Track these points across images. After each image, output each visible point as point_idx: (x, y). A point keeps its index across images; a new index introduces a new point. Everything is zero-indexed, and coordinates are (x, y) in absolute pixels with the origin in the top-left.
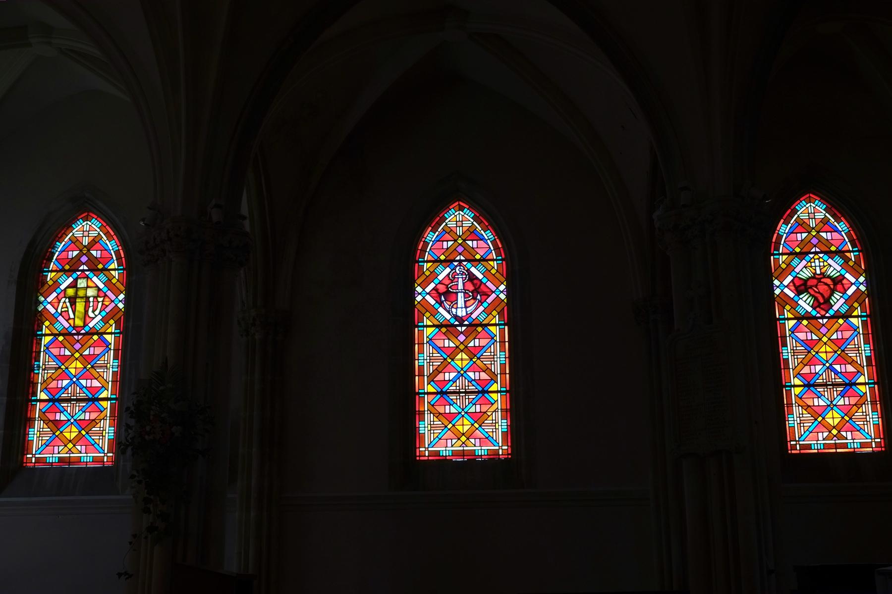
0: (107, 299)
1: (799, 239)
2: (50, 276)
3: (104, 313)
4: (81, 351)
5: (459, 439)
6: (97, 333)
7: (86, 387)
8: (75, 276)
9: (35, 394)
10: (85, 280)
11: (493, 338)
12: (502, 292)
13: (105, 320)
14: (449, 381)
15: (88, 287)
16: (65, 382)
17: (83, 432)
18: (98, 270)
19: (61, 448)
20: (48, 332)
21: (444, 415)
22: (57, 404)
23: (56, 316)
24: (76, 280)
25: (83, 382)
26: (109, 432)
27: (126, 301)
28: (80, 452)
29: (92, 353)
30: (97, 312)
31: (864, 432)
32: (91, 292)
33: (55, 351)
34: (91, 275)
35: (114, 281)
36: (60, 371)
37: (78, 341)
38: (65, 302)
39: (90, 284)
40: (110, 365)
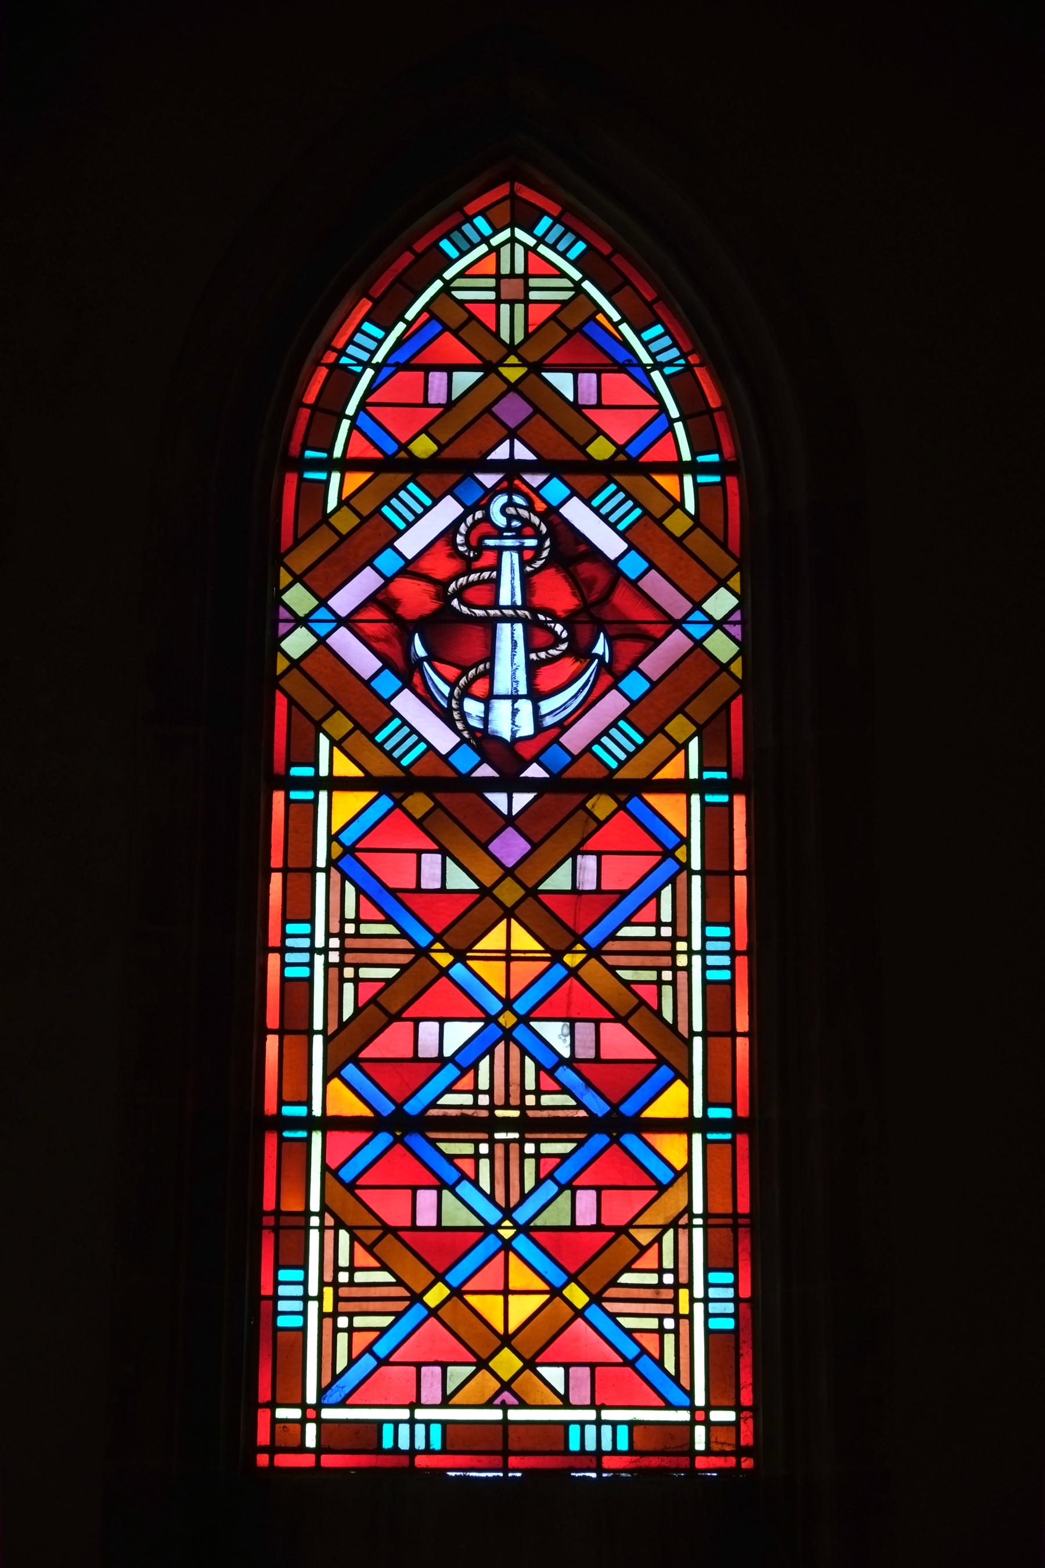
5: (482, 1364)
11: (668, 853)
12: (718, 625)
14: (441, 1061)
17: (577, 1296)
19: (457, 1374)
26: (712, 1300)
28: (566, 1403)
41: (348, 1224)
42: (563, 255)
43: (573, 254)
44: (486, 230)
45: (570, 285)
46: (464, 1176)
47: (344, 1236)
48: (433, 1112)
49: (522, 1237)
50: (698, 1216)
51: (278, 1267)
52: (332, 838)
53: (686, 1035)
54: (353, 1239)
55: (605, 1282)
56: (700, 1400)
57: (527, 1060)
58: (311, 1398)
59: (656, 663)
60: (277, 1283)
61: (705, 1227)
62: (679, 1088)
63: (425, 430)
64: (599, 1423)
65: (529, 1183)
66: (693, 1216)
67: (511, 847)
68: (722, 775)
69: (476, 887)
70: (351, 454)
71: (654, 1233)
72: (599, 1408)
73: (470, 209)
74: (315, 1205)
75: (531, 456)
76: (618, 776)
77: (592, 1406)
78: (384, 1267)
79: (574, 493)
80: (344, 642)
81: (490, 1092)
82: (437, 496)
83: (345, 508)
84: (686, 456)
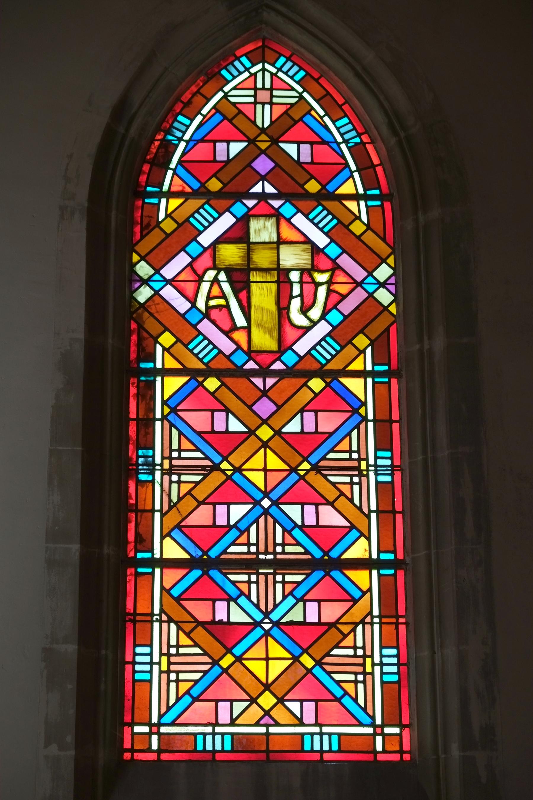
0: (341, 278)
1: (221, 156)
2: (166, 207)
3: (335, 317)
4: (276, 422)
5: (253, 700)
6: (321, 372)
7: (303, 527)
8: (239, 209)
9: (144, 542)
10: (271, 223)
11: (355, 411)
12: (382, 285)
13: (341, 335)
14: (229, 527)
15: (280, 241)
16: (238, 511)
17: (308, 662)
18: (307, 195)
19: (239, 707)
20: (171, 363)
21: (214, 627)
22: (215, 574)
23: (194, 317)
24: (243, 223)
25: (294, 511)
26: (385, 663)
27: (399, 284)
28: (301, 722)
29: (310, 427)
30: (315, 313)
31: (355, 699)
32: (292, 257)
33: (199, 420)
34: (288, 210)
35: (357, 228)
36: (216, 478)
37: (265, 393)
38: (215, 281)
39: (287, 233)
40: (367, 467)
41: (175, 620)
42: (292, 78)
43: (298, 78)
44: (248, 64)
45: (297, 95)
46: (242, 593)
47: (173, 627)
48: (223, 557)
49: (275, 628)
50: (376, 617)
51: (135, 645)
52: (164, 403)
53: (366, 512)
54: (179, 629)
55: (324, 653)
56: (379, 721)
57: (277, 526)
58: (155, 720)
59: (347, 306)
60: (135, 654)
61: (380, 624)
62: (363, 542)
63: (215, 175)
64: (321, 734)
65: (279, 598)
66: (373, 617)
67: (263, 165)
68: (386, 368)
69: (246, 430)
70: (173, 189)
71: (351, 627)
72: (321, 726)
73: (238, 53)
74: (157, 610)
75: (274, 191)
76: (325, 368)
77: (316, 724)
78: (196, 645)
79: (299, 211)
80: (169, 293)
81: (257, 545)
82: (221, 212)
83: (169, 219)
84: (361, 191)
